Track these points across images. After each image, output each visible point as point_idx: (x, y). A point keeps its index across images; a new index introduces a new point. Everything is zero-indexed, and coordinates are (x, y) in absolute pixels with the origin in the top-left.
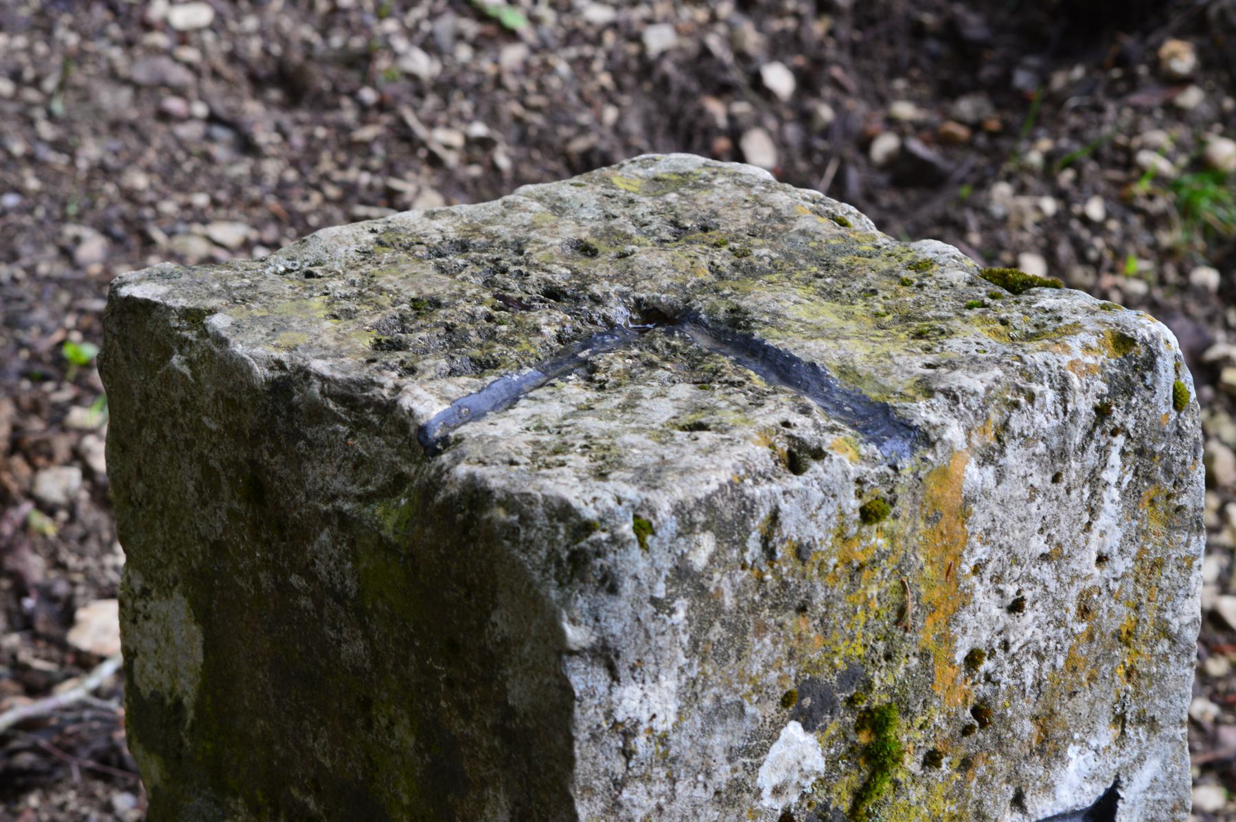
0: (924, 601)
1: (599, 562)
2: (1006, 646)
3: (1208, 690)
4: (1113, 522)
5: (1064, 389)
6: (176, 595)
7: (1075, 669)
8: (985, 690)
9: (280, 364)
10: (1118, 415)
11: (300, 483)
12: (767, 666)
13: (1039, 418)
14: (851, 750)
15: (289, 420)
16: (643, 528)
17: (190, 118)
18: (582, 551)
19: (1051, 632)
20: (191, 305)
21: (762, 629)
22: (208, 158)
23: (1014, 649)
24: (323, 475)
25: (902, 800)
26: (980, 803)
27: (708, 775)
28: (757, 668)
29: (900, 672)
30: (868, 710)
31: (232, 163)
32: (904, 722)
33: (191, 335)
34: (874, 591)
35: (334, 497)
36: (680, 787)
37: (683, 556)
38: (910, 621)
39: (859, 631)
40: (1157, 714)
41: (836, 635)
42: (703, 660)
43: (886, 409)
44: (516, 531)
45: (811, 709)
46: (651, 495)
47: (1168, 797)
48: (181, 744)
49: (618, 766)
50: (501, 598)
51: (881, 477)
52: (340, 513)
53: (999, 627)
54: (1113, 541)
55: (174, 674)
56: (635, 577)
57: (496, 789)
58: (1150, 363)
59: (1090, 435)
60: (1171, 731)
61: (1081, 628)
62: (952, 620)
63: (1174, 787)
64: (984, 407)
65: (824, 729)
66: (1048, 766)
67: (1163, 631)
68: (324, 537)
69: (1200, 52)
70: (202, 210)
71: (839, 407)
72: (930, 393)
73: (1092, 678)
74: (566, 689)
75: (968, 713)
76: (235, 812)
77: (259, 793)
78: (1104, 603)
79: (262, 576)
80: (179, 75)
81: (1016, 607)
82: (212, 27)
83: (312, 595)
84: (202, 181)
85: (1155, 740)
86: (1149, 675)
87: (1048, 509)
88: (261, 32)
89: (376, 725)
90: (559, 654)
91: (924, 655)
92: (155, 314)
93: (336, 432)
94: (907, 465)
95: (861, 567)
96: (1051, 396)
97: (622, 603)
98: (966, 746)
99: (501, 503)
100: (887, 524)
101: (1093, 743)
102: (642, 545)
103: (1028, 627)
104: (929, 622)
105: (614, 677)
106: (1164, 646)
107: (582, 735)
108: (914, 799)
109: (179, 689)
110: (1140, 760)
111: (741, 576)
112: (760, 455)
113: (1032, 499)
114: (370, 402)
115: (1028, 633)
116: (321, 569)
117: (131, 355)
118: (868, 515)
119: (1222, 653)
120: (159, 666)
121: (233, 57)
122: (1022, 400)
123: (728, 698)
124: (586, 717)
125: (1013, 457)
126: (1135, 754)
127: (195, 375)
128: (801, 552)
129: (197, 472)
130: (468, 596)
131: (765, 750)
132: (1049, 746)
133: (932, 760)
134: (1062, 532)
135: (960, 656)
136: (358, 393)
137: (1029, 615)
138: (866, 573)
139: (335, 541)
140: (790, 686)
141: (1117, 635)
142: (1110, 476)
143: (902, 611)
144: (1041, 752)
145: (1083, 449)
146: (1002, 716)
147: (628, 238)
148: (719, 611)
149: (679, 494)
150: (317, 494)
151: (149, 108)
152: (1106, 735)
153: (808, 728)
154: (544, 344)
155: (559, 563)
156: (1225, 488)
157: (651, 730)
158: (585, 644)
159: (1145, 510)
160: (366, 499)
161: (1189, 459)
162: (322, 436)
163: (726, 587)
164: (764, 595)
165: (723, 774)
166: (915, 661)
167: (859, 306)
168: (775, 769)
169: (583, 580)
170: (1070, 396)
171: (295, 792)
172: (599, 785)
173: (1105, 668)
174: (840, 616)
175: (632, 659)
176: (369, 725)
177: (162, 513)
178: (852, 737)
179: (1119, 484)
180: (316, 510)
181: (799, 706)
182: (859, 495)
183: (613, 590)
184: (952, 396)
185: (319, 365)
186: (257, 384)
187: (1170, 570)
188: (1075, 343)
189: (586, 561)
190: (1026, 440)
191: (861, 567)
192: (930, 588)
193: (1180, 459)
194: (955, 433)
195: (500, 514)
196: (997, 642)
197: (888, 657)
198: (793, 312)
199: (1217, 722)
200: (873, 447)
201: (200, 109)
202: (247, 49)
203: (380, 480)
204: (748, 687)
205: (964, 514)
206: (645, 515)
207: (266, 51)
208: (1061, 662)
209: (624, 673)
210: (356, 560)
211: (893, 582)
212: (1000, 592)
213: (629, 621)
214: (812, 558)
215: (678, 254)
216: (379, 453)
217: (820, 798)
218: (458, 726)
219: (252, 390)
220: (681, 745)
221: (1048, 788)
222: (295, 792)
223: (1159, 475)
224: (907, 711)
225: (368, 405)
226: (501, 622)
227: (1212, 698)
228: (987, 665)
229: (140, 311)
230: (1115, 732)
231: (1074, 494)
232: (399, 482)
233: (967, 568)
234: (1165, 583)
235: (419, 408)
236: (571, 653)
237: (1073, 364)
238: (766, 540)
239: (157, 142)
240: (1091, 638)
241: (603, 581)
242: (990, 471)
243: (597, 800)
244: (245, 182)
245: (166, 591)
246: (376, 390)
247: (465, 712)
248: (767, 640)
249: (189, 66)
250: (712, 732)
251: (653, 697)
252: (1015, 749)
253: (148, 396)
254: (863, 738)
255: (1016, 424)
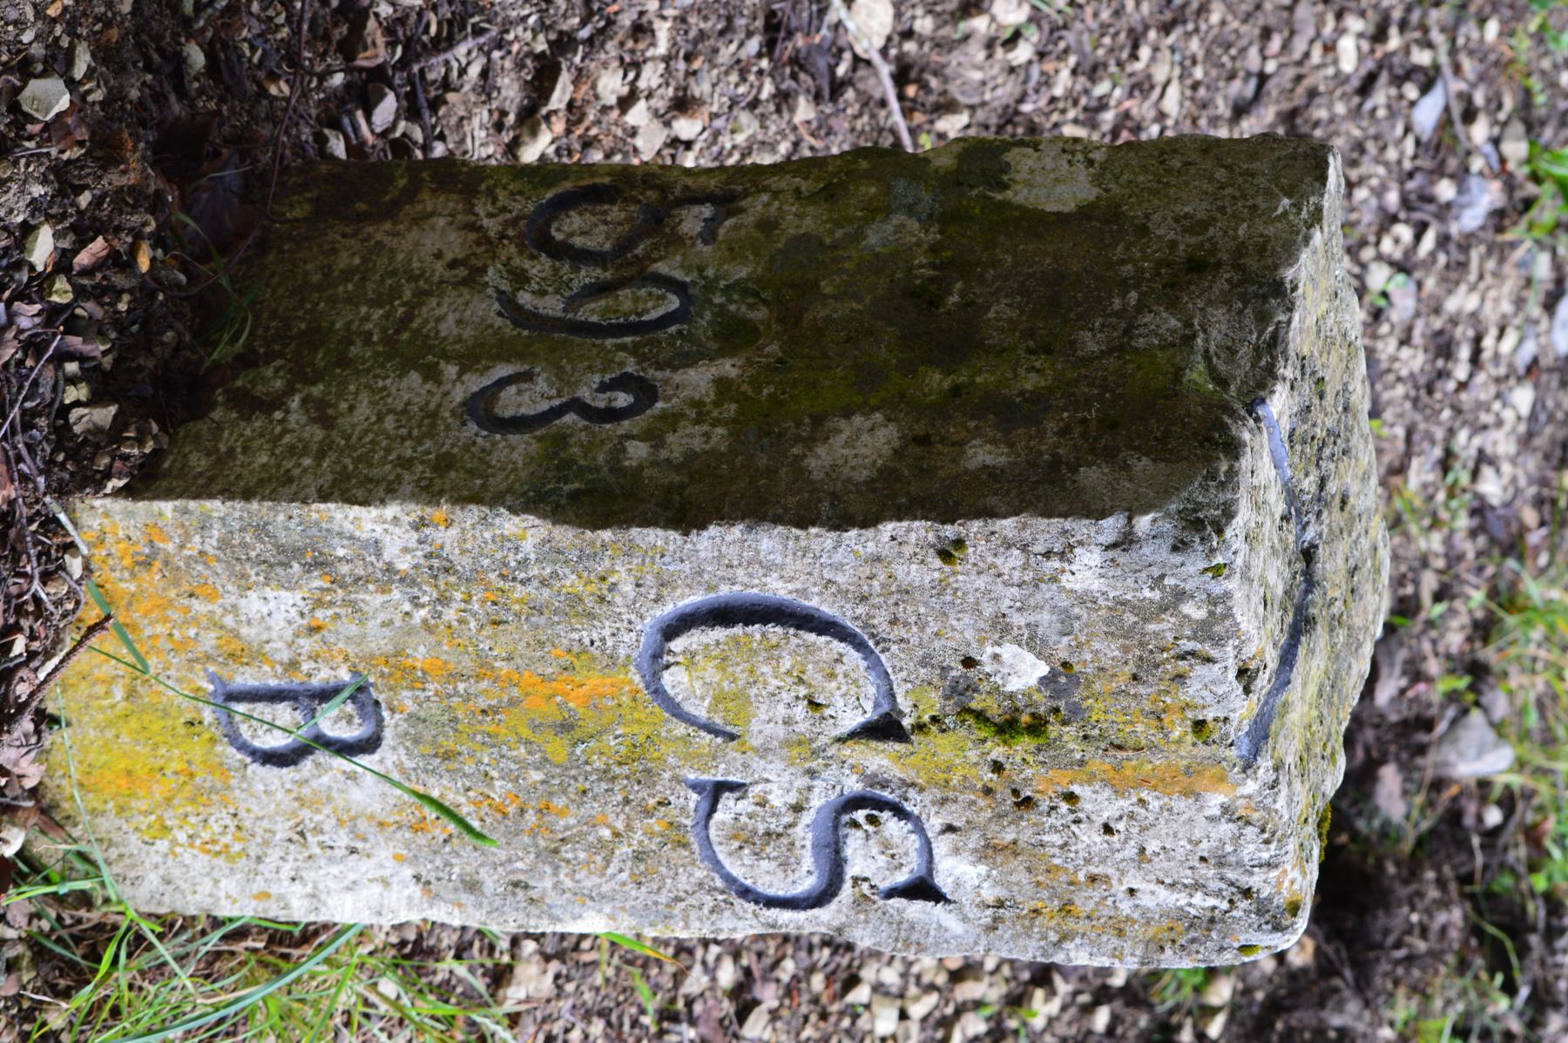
0: (1125, 763)
1: (1197, 540)
2: (1077, 822)
3: (801, 974)
4: (1160, 900)
5: (1269, 865)
6: (1096, 191)
7: (1048, 871)
8: (1044, 806)
9: (1295, 288)
10: (1244, 904)
11: (1210, 303)
12: (1096, 652)
13: (1252, 847)
14: (1017, 710)
15: (1256, 296)
16: (1217, 571)
17: (1264, 58)
18: (1205, 528)
19: (1083, 854)
20: (1325, 212)
21: (1126, 649)
22: (1232, 76)
23: (1074, 828)
24: (1219, 322)
25: (970, 745)
26: (955, 801)
27: (1020, 609)
28: (1096, 645)
29: (1071, 746)
30: (1047, 722)
31: (1226, 98)
32: (1032, 748)
33: (1304, 214)
34: (1140, 728)
35: (1205, 331)
36: (1015, 590)
37: (1192, 597)
38: (1112, 752)
39: (1111, 717)
40: (999, 932)
41: (1110, 701)
42: (1110, 609)
43: (1266, 737)
44: (1214, 478)
45: (1056, 682)
46: (1238, 575)
47: (931, 939)
48: (972, 187)
49: (1039, 548)
50: (1162, 465)
51: (1227, 734)
52: (1194, 336)
53: (1094, 817)
54: (1146, 900)
55: (1029, 185)
56: (1183, 564)
57: (1008, 455)
58: (1278, 928)
59: (1232, 884)
60: (983, 941)
61: (1081, 876)
62: (1106, 783)
63: (937, 944)
64: (1264, 808)
65: (1039, 691)
66: (975, 851)
67: (1065, 937)
68: (1173, 322)
69: (1304, 971)
70: (1190, 75)
71: (1266, 703)
72: (1276, 769)
73: (1038, 884)
74: (1102, 514)
75: (1029, 793)
76: (927, 231)
77: (949, 253)
78: (1097, 893)
79: (1129, 267)
80: (1300, 45)
81: (1108, 829)
82: (1338, 73)
83: (1124, 310)
84: (1214, 72)
85: (978, 930)
86: (1032, 926)
87: (1180, 854)
88: (1332, 120)
89: (1033, 357)
90: (1129, 509)
91: (1082, 763)
92: (1317, 185)
93: (1251, 332)
94: (1233, 753)
95: (1159, 718)
96: (1265, 856)
97: (1164, 555)
98: (1003, 793)
99: (1231, 467)
100: (1190, 738)
101: (985, 885)
102: (1206, 570)
103: (1089, 837)
104: (1107, 767)
105: (1108, 548)
106: (1053, 937)
107: (1068, 524)
108: (969, 754)
109: (1018, 187)
110: (965, 919)
111: (1170, 636)
112: (1250, 650)
113: (1190, 841)
114: (1274, 358)
115: (1084, 838)
116: (1148, 318)
117: (1282, 163)
118: (1199, 725)
119: (827, 987)
120: (1032, 171)
121: (1313, 94)
122: (1266, 836)
123: (1077, 625)
124: (1081, 528)
125: (1226, 829)
126: (971, 916)
127: (1278, 218)
128: (1180, 678)
129: (1202, 215)
130: (1156, 439)
131: (1031, 649)
132: (990, 852)
133: (997, 767)
134: (1160, 864)
135: (1076, 789)
136: (1280, 349)
137: (1099, 838)
138: (1155, 723)
139: (1173, 331)
140: (1077, 668)
141: (1070, 902)
142: (1198, 898)
143: (1120, 748)
144: (987, 846)
145: (1222, 879)
146: (1021, 818)
147: (1350, 534)
148: (1145, 620)
149: (1237, 595)
150: (1204, 316)
151: (1272, 21)
152: (989, 893)
153: (1043, 680)
154: (1299, 481)
155: (1195, 511)
156: (952, 990)
157: (1063, 571)
158: (1136, 529)
159: (1165, 923)
160: (1207, 357)
161: (1200, 957)
162: (1247, 322)
163: (1164, 626)
164: (1151, 652)
165: (1018, 620)
166: (1078, 756)
167: (1315, 713)
168: (1015, 656)
169: (1184, 528)
170: (1264, 869)
171: (959, 285)
172: (1027, 535)
173: (1045, 894)
174: (1125, 704)
175: (1121, 560)
176: (1030, 351)
177: (1159, 182)
178: (1028, 710)
179: (1190, 905)
180: (1193, 317)
181: (1060, 674)
182: (1216, 720)
183: (1175, 549)
184: (1274, 785)
185: (1296, 317)
186: (1281, 271)
187: (1115, 942)
188: (1295, 874)
189: (1198, 531)
190: (1237, 838)
191: (1159, 718)
192: (1135, 768)
193: (1202, 949)
194: (1251, 787)
195: (1224, 467)
196: (1081, 815)
197: (1085, 737)
198: (1314, 664)
199: (778, 981)
200: (1247, 729)
201: (1271, 67)
202: (1319, 106)
203: (1222, 367)
204: (1083, 639)
205: (1186, 793)
206: (1226, 572)
207: (1316, 124)
208: (1057, 861)
209: (1110, 554)
210: (1162, 348)
211: (1144, 742)
212: (1121, 818)
213: (1150, 559)
214: (1174, 685)
215: (1341, 577)
216: (1239, 366)
217: (984, 687)
218: (1051, 426)
219: (1276, 267)
220: (1048, 590)
221: (956, 851)
222: (959, 285)
223: (1192, 934)
224: (1039, 750)
225: (1272, 357)
226: (1142, 464)
227: (795, 977)
228: (1064, 807)
229: (1318, 172)
230: (991, 900)
231: (1189, 872)
232: (1223, 383)
233: (1144, 795)
234: (1105, 938)
235: (1276, 397)
236: (1130, 519)
237: (1285, 872)
238: (1193, 654)
239: (1244, 29)
240: (1072, 883)
241: (1182, 542)
242: (1217, 812)
243: (1015, 532)
244: (1210, 112)
245: (1097, 180)
246: (1282, 363)
247: (1063, 432)
248: (1117, 653)
249: (1307, 55)
250: (1053, 613)
251: (1088, 574)
252: (994, 827)
253: (1253, 175)
254: (1025, 718)
255: (1250, 832)
